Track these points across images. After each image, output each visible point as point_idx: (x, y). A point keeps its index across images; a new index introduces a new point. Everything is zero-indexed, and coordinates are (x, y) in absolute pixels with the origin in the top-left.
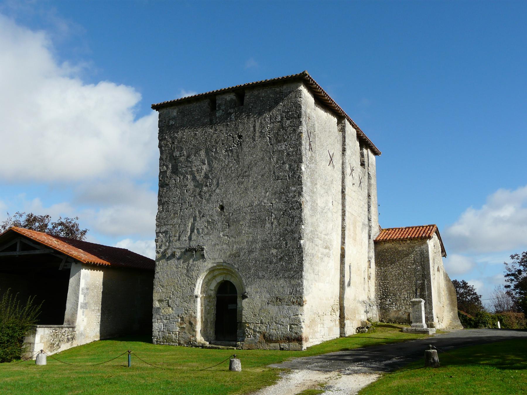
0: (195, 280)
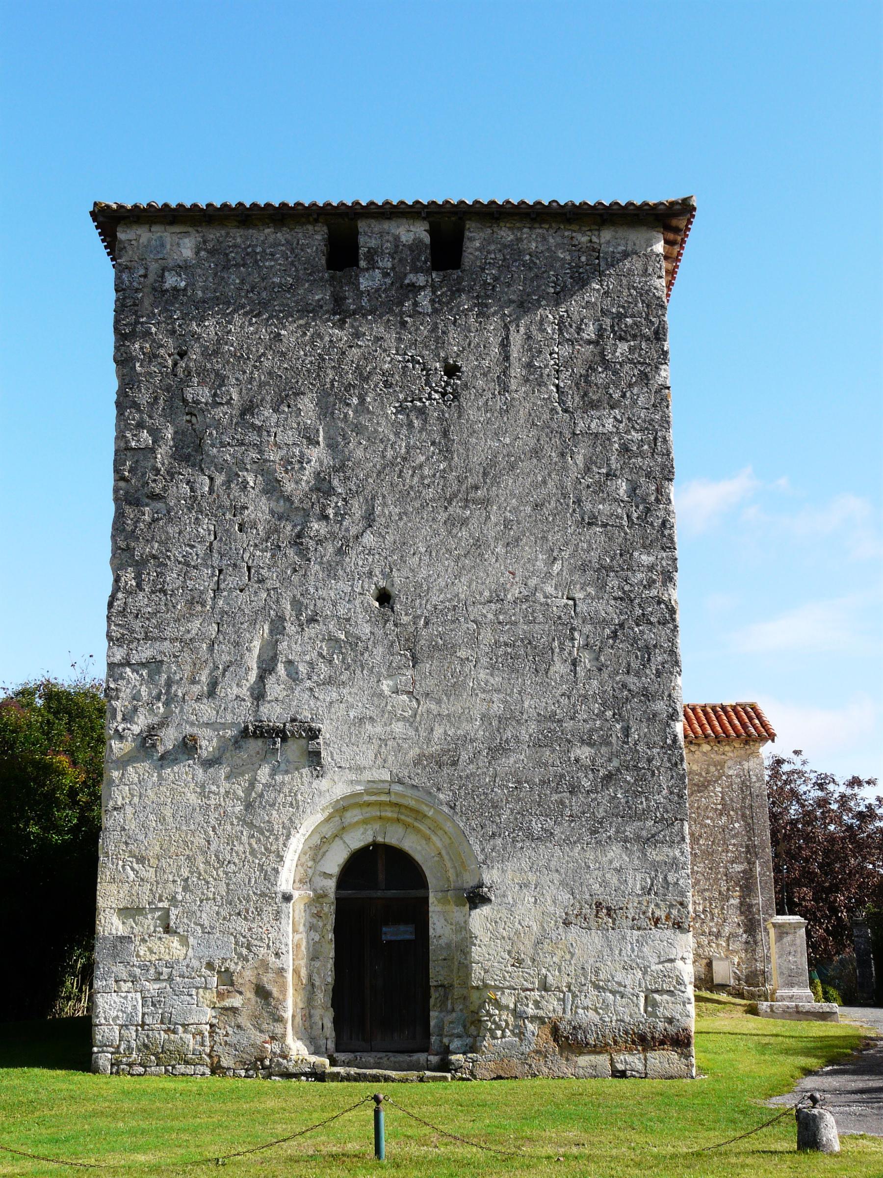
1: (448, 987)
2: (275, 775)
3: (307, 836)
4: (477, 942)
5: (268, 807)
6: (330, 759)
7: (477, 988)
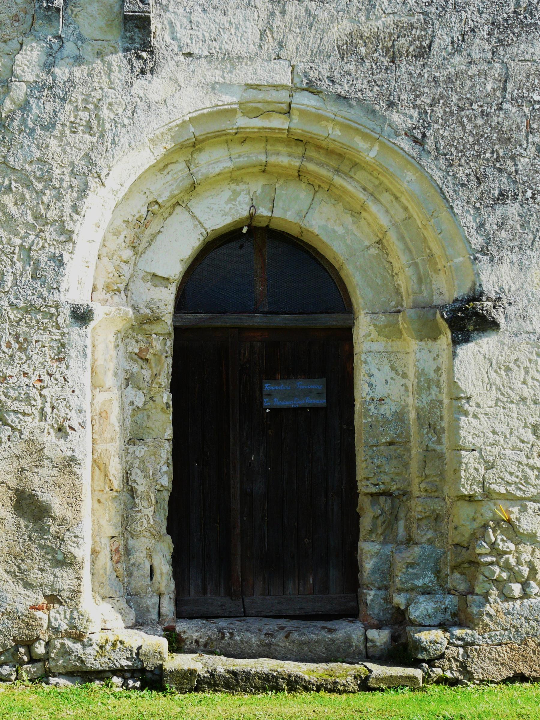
0: (69, 198)
1: (398, 497)
2: (53, 64)
3: (121, 195)
4: (471, 409)
5: (38, 130)
6: (168, 38)
7: (470, 499)
